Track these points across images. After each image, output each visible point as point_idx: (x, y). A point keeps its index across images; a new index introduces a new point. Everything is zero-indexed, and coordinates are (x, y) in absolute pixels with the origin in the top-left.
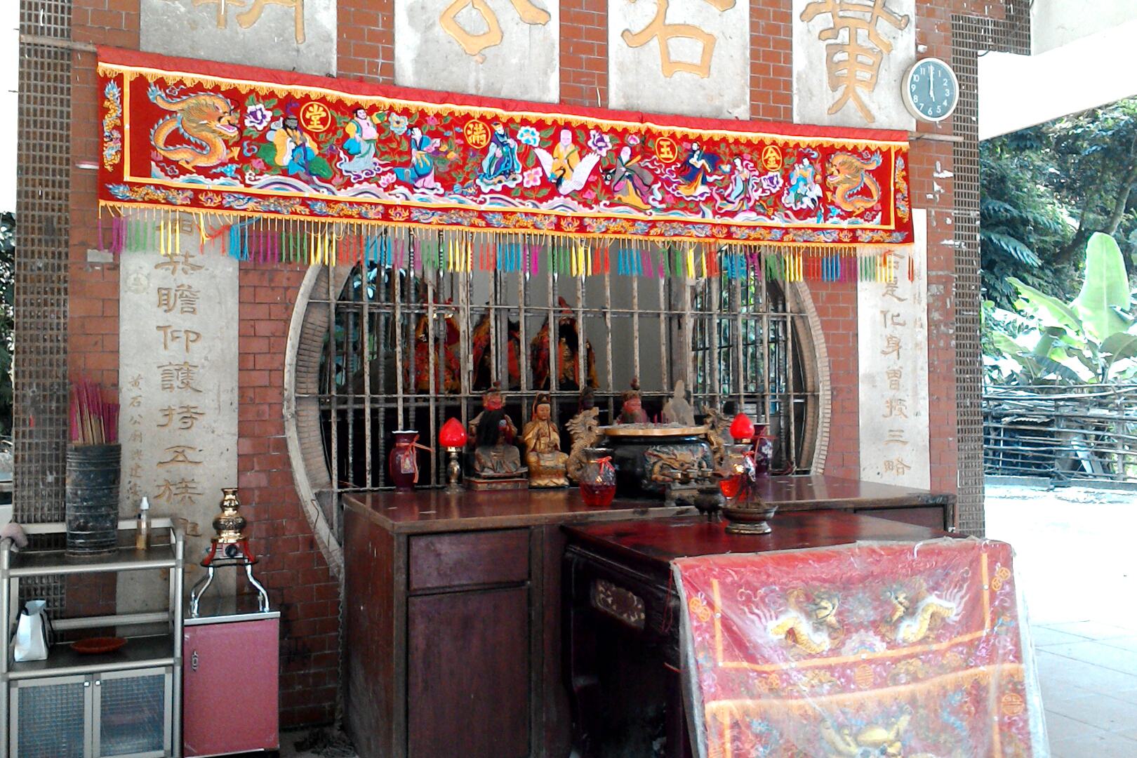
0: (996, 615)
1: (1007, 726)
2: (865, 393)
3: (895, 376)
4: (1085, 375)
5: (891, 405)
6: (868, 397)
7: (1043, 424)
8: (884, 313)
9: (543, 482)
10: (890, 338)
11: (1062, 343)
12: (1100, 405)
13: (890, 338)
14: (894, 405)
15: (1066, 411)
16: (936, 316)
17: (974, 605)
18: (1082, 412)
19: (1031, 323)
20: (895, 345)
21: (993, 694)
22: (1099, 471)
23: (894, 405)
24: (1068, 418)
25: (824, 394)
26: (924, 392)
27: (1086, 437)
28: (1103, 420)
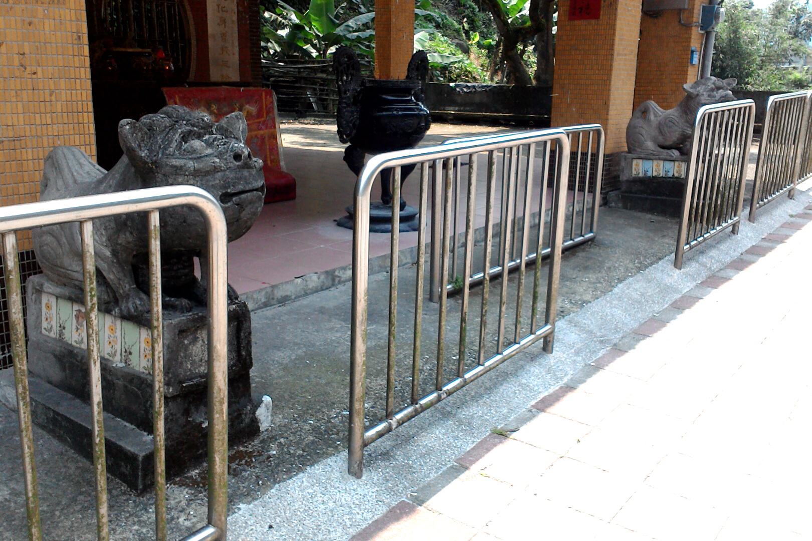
0: (267, 113)
1: (271, 150)
2: (211, 43)
3: (223, 35)
4: (314, 54)
5: (222, 49)
6: (212, 44)
7: (292, 82)
8: (218, 6)
9: (146, 35)
10: (221, 18)
11: (301, 35)
12: (322, 72)
13: (221, 18)
14: (223, 49)
15: (304, 75)
16: (240, 8)
17: (260, 111)
18: (313, 75)
19: (286, 22)
20: (223, 21)
21: (266, 139)
22: (321, 109)
23: (223, 49)
24: (305, 79)
25: (194, 42)
26: (236, 44)
27: (315, 89)
28: (324, 80)
